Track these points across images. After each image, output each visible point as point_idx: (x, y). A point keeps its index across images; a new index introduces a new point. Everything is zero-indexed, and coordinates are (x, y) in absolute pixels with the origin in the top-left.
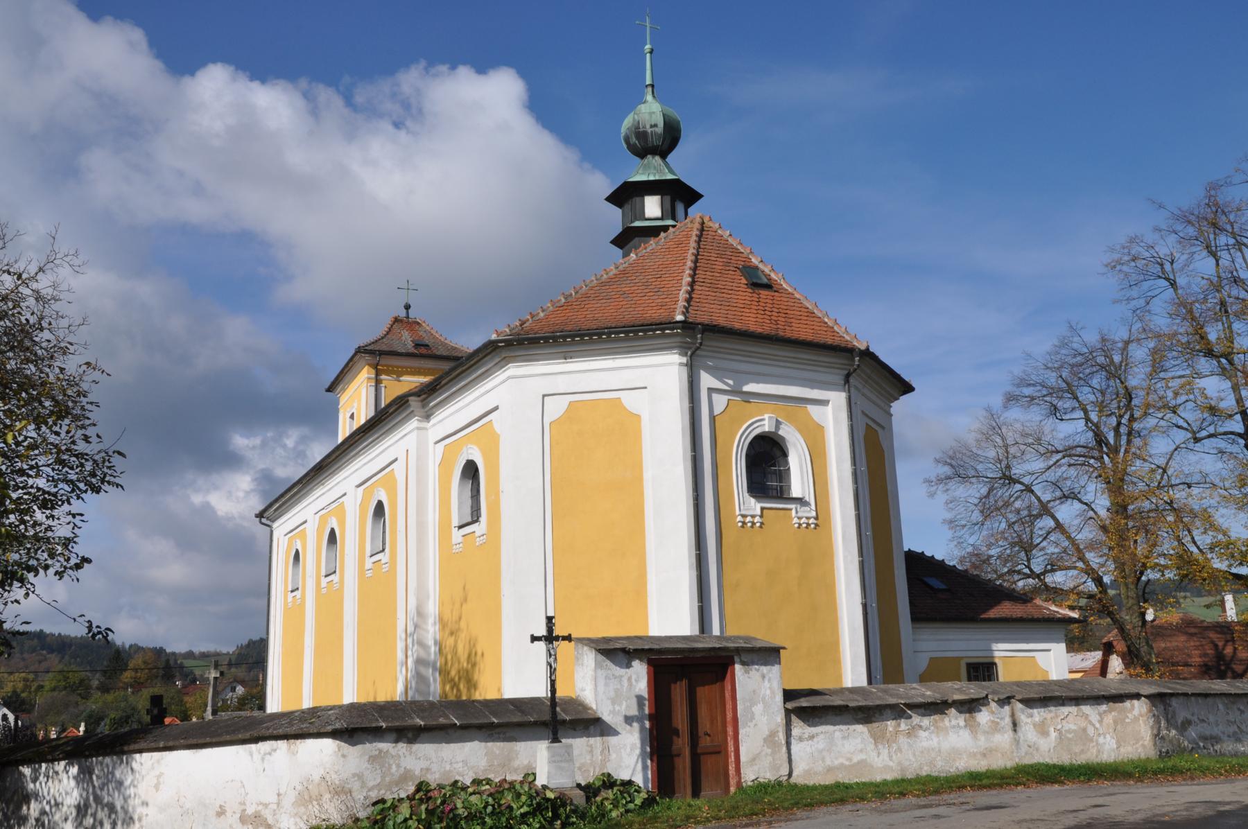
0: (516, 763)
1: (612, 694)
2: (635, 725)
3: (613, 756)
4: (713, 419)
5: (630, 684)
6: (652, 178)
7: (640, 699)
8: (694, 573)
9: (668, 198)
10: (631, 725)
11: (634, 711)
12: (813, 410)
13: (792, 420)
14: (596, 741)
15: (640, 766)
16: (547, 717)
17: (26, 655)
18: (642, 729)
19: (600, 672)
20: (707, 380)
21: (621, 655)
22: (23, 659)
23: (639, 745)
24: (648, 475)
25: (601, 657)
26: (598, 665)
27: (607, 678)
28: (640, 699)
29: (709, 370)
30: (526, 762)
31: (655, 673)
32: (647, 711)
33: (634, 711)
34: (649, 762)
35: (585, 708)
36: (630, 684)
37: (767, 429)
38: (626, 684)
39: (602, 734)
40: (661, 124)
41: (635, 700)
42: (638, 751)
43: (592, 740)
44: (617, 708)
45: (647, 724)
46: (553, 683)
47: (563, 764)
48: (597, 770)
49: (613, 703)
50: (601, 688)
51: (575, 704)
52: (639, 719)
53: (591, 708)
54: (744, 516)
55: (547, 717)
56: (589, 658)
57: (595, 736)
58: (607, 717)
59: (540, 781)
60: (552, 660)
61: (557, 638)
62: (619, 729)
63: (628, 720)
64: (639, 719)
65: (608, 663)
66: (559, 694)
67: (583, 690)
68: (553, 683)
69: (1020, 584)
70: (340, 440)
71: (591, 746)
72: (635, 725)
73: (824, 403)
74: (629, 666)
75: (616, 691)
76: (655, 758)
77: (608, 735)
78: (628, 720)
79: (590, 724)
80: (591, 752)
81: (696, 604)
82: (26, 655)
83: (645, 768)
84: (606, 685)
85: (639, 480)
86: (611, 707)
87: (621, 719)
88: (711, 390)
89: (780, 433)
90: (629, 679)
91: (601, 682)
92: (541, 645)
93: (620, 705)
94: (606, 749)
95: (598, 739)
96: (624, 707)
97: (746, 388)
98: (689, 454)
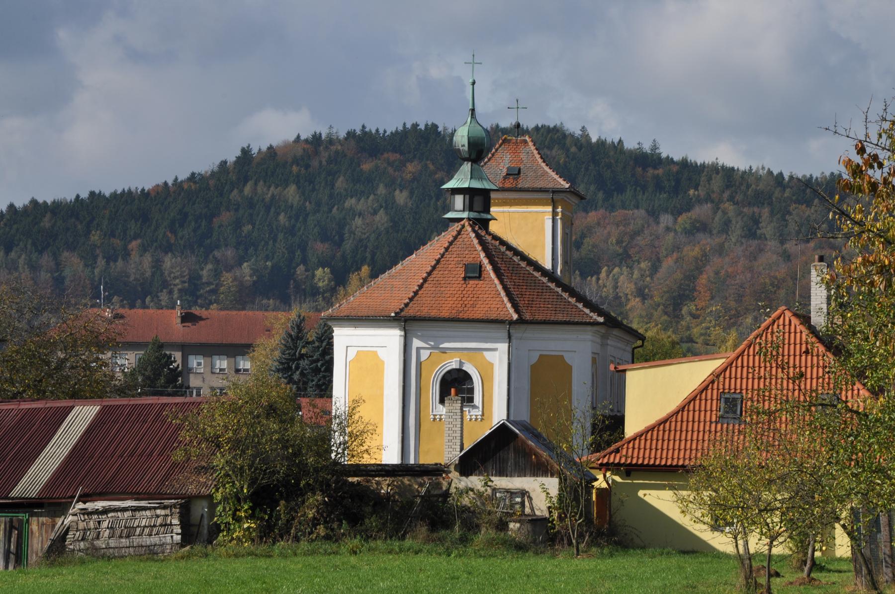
4: (419, 364)
6: (25, 479)
9: (467, 197)
12: (487, 354)
13: (470, 361)
17: (791, 246)
20: (416, 343)
22: (787, 257)
24: (385, 393)
29: (418, 337)
37: (454, 367)
40: (467, 145)
54: (435, 415)
69: (245, 491)
73: (495, 350)
82: (791, 246)
85: (382, 395)
88: (418, 349)
89: (464, 368)
97: (441, 346)
98: (402, 384)
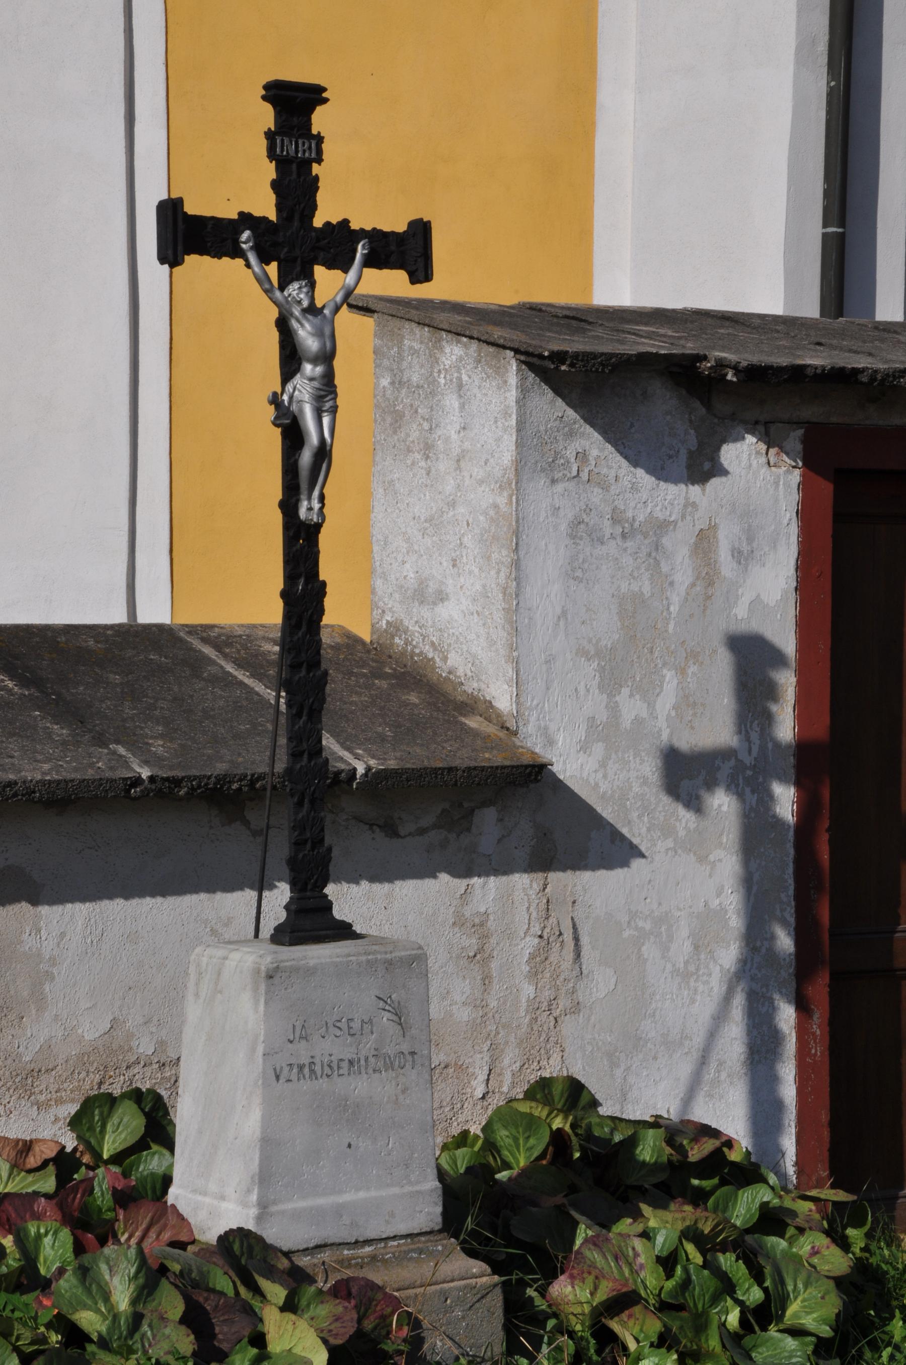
0: (35, 1036)
1: (606, 627)
2: (722, 803)
3: (600, 983)
5: (707, 575)
7: (751, 656)
8: (818, 85)
10: (694, 804)
11: (715, 727)
14: (509, 897)
15: (734, 1041)
16: (260, 755)
18: (756, 827)
19: (543, 497)
21: (663, 405)
23: (736, 922)
25: (550, 407)
26: (535, 456)
27: (580, 529)
28: (751, 656)
30: (91, 1030)
31: (842, 517)
32: (786, 728)
33: (715, 727)
34: (786, 1016)
35: (444, 702)
36: (707, 575)
38: (682, 569)
39: (544, 859)
41: (721, 669)
42: (729, 955)
43: (487, 891)
44: (631, 708)
45: (785, 800)
46: (301, 544)
47: (359, 1086)
48: (510, 1060)
49: (611, 681)
50: (546, 590)
51: (411, 684)
52: (745, 773)
53: (487, 710)
55: (260, 755)
56: (483, 407)
57: (500, 867)
58: (573, 766)
59: (212, 1195)
60: (302, 389)
61: (338, 244)
62: (635, 831)
63: (685, 774)
64: (745, 773)
65: (592, 443)
66: (340, 614)
67: (424, 594)
68: (301, 544)
70: (257, 1277)
71: (479, 927)
72: (722, 803)
74: (703, 467)
75: (631, 609)
76: (820, 989)
77: (579, 861)
78: (685, 774)
79: (497, 807)
80: (480, 957)
81: (814, 230)
83: (762, 1048)
84: (576, 572)
86: (595, 704)
87: (649, 768)
90: (704, 541)
91: (548, 557)
92: (233, 285)
93: (648, 691)
94: (561, 943)
95: (522, 883)
96: (667, 700)
